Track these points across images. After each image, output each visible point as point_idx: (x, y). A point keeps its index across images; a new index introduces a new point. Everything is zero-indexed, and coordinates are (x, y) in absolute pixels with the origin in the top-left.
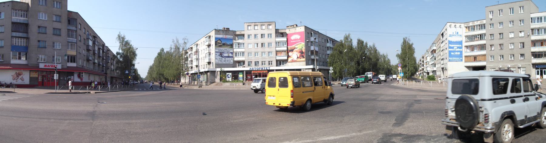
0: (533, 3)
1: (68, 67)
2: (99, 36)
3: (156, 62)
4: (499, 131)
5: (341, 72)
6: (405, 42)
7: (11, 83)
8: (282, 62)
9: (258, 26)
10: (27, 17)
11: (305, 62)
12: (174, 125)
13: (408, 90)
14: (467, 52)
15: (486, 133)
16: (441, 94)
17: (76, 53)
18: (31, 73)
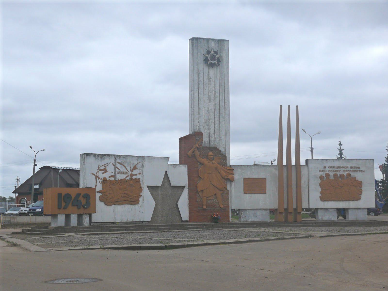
0: (230, 187)
1: (181, 163)
2: (332, 202)
3: (3, 228)
4: (192, 118)
5: (98, 179)
6: (147, 186)
7: (133, 171)
8: (185, 215)
9: (203, 165)
10: (25, 204)
11: (308, 207)
12: (232, 234)
13: (48, 216)
14: (295, 221)
15: (134, 179)
16: (58, 282)
17: (311, 157)
18: (264, 212)
